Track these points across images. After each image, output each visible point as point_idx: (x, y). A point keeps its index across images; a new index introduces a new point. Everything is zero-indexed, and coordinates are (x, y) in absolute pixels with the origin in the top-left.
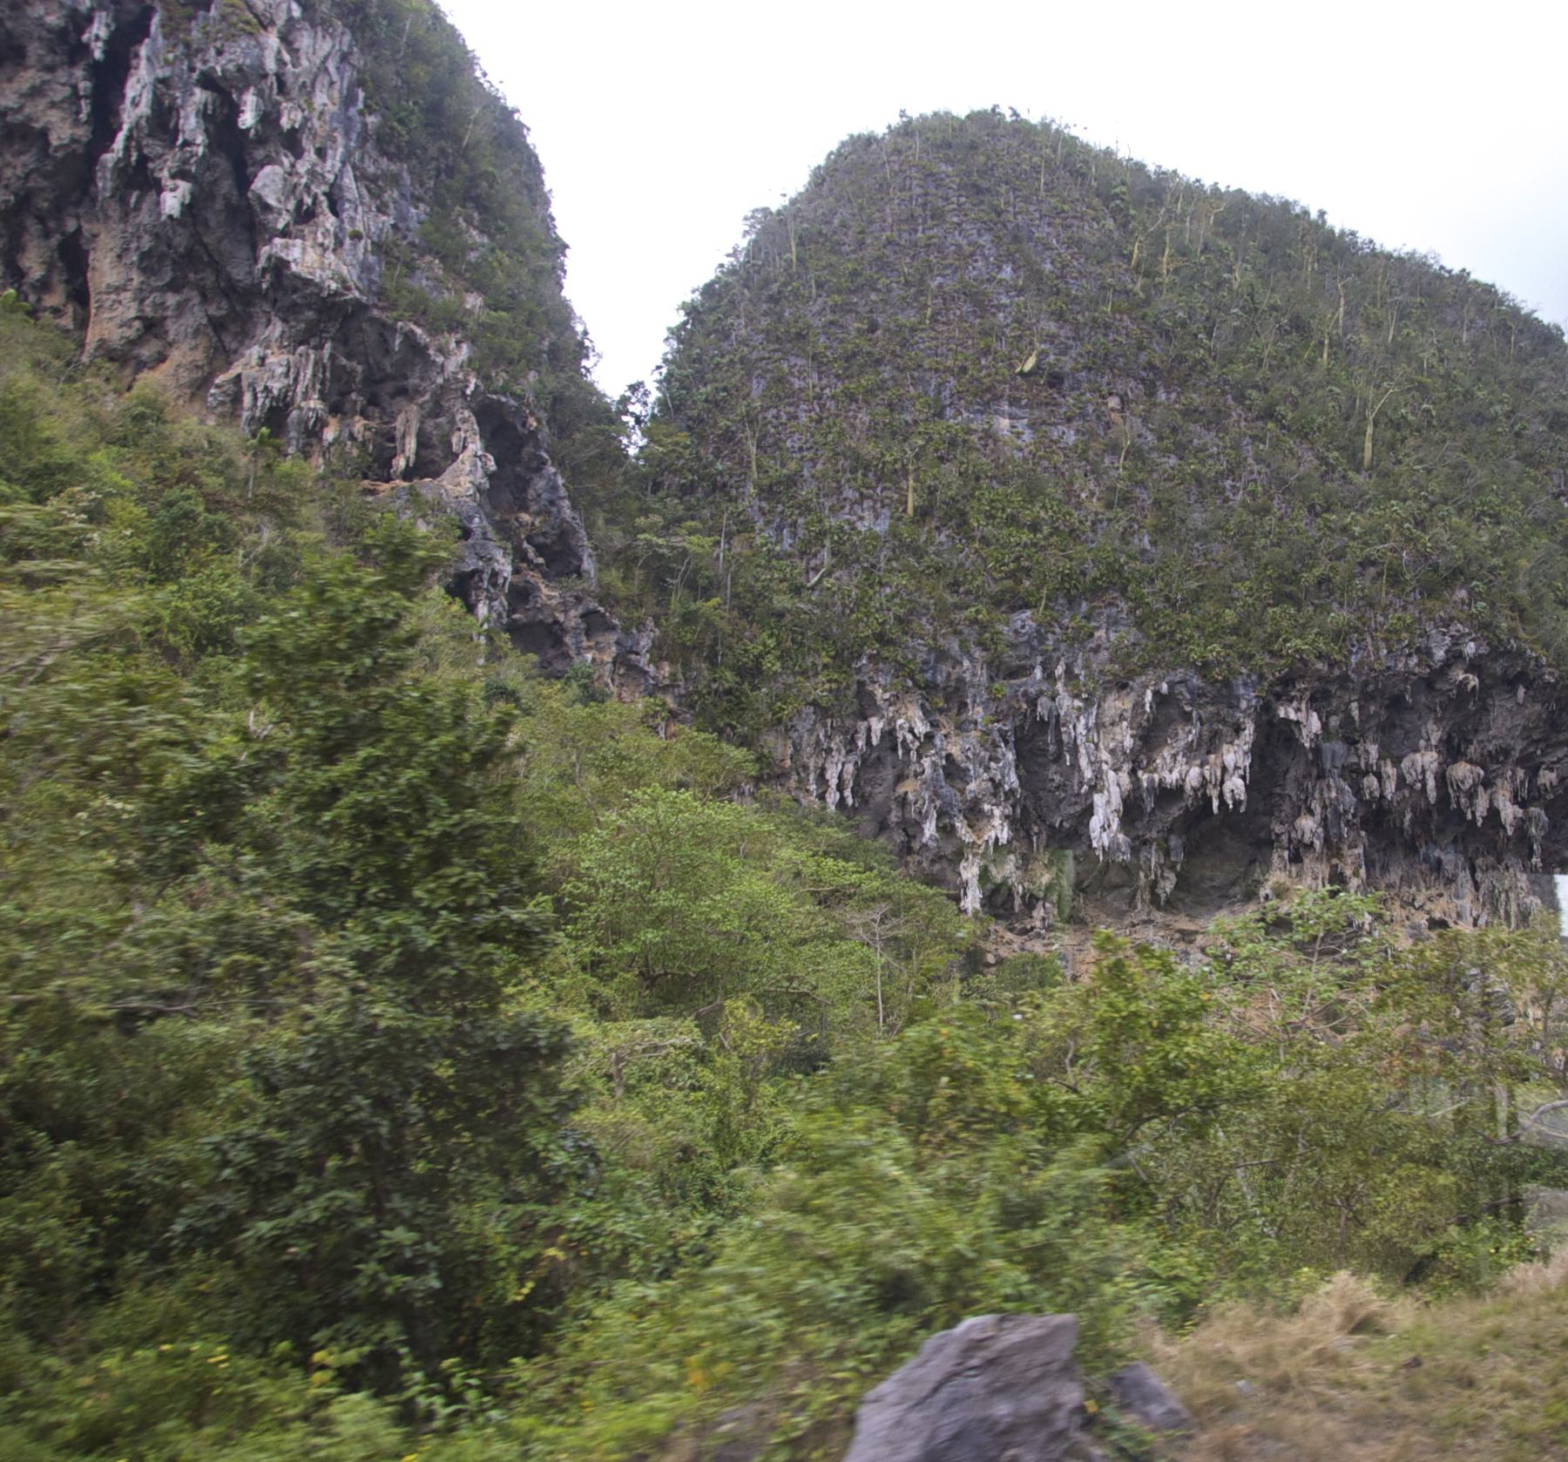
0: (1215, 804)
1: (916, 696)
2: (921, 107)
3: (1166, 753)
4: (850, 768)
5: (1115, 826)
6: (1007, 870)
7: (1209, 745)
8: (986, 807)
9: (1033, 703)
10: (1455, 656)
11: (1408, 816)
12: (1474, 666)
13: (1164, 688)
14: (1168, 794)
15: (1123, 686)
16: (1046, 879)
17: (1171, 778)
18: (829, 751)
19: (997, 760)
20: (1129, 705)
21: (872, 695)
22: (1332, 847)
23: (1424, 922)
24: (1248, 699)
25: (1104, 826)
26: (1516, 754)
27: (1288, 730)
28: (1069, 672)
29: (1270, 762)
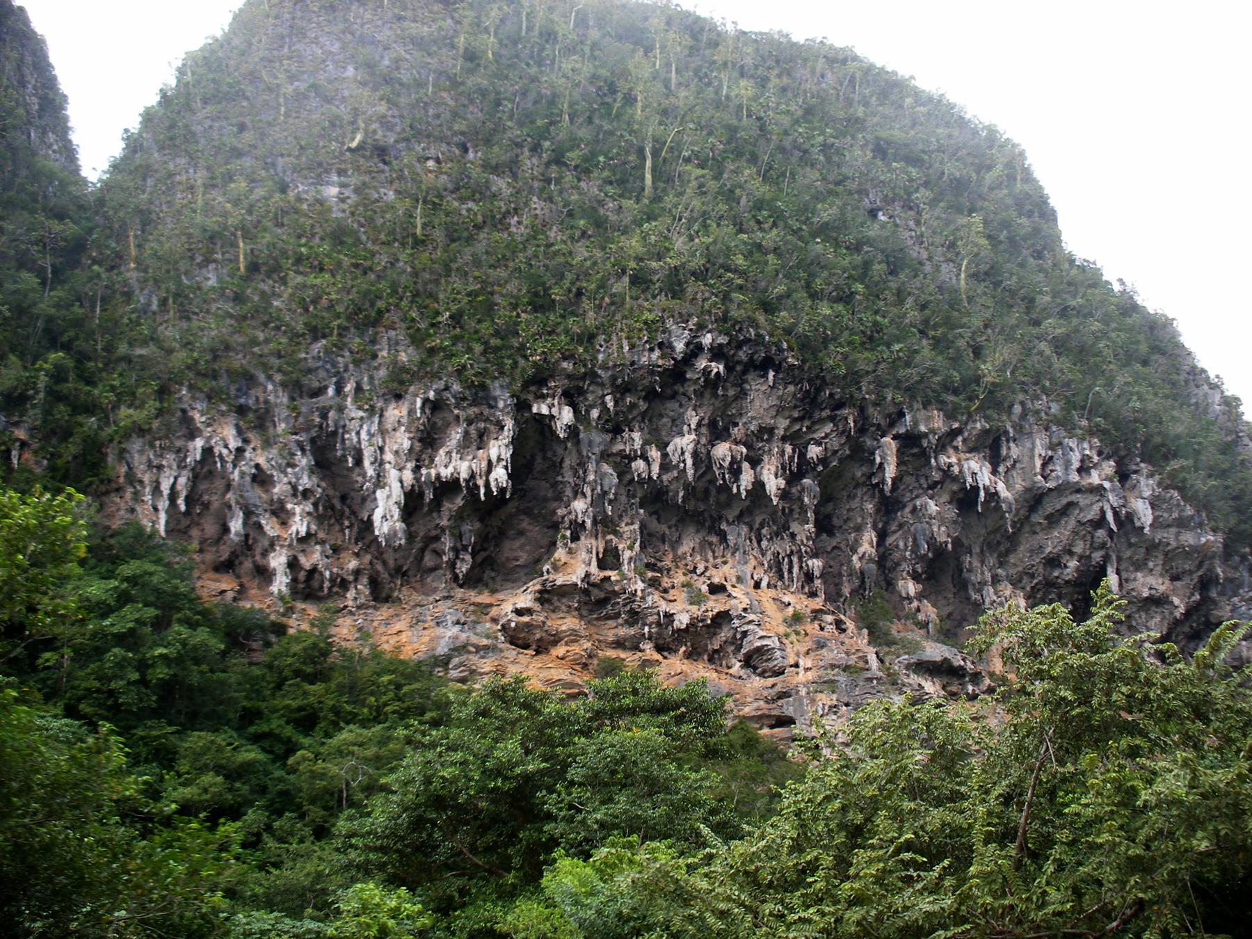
0: (482, 491)
1: (232, 419)
2: (952, 97)
3: (442, 452)
4: (182, 481)
5: (396, 516)
6: (314, 557)
7: (481, 440)
8: (289, 506)
9: (324, 416)
10: (695, 349)
11: (681, 494)
12: (717, 353)
13: (431, 395)
14: (448, 487)
15: (398, 397)
16: (353, 564)
17: (446, 473)
18: (160, 468)
19: (293, 466)
20: (405, 412)
21: (192, 419)
22: (605, 524)
23: (705, 588)
24: (504, 400)
25: (385, 515)
26: (780, 432)
27: (544, 424)
28: (359, 389)
29: (549, 454)
